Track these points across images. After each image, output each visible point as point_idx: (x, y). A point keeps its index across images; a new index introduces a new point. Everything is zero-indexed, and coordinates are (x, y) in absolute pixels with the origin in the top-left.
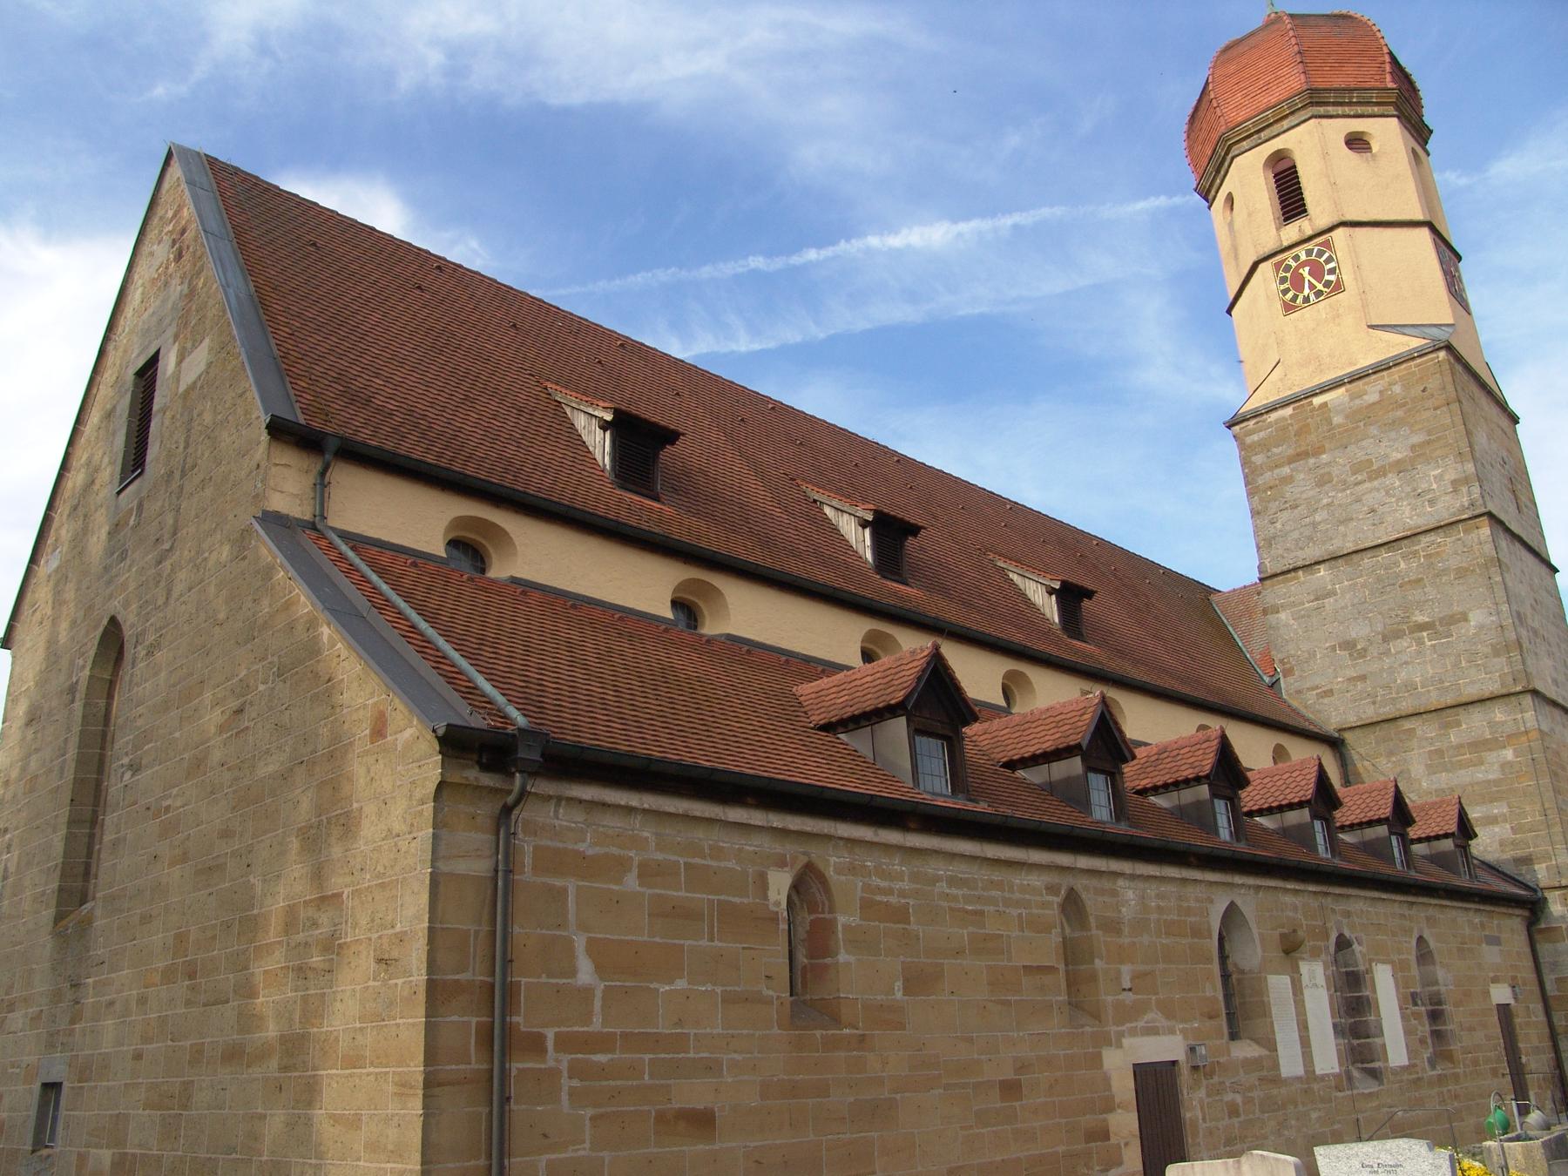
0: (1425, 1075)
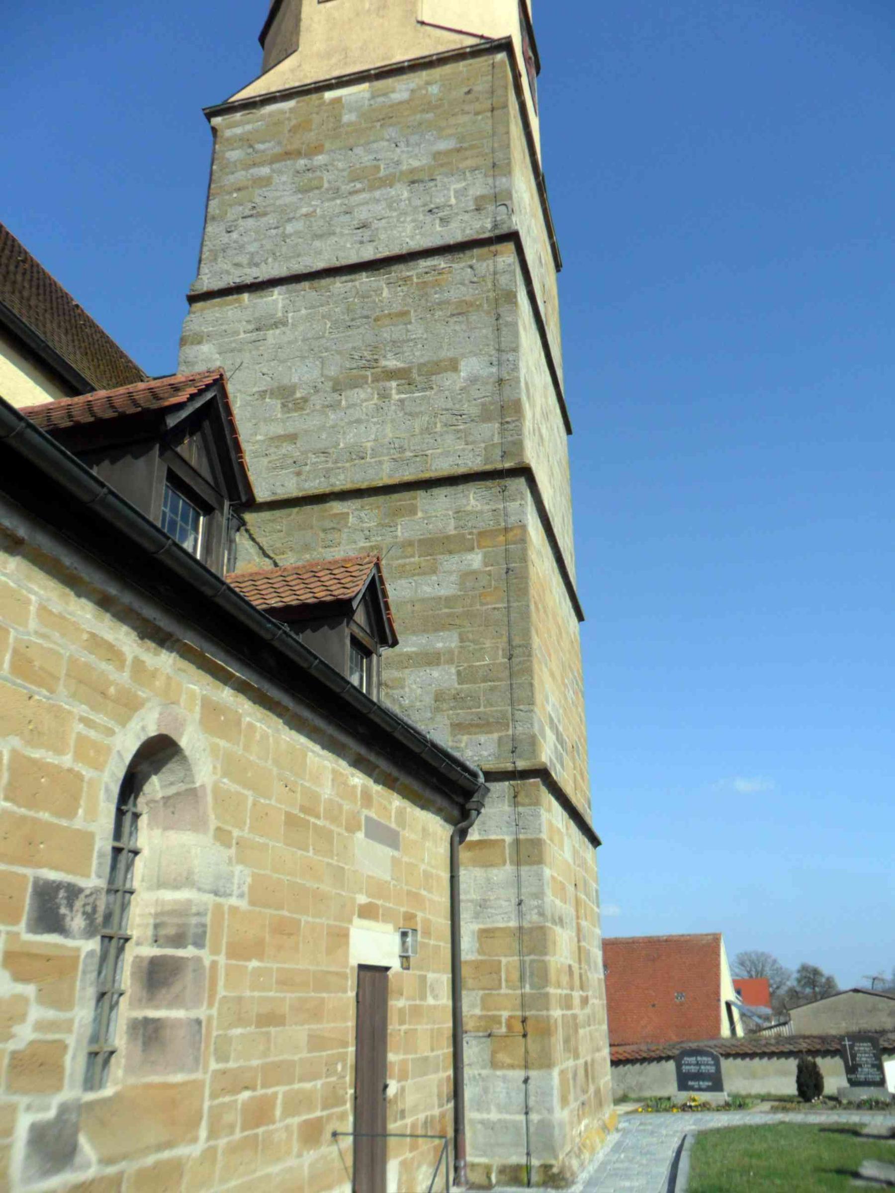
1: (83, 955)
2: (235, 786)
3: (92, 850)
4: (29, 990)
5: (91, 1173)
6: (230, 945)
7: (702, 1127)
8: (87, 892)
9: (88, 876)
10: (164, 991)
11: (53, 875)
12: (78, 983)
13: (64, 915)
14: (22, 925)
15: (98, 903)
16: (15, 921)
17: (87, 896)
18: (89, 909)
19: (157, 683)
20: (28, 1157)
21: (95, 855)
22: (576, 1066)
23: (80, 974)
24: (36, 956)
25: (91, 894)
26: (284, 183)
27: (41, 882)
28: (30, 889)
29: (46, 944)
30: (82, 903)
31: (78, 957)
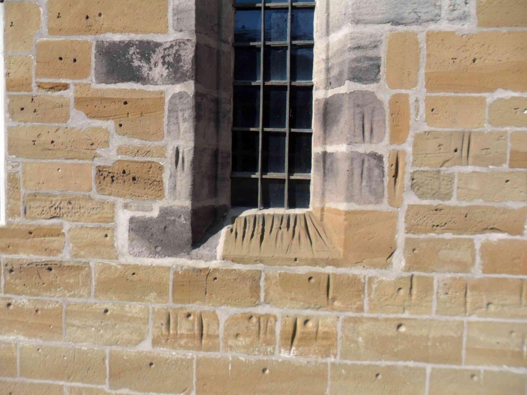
0: (94, 263)
1: (167, 100)
2: (44, 257)
3: (166, 9)
4: (110, 125)
5: (213, 264)
6: (428, 78)
7: (474, 170)
8: (168, 45)
9: (165, 31)
10: (335, 128)
11: (117, 38)
12: (165, 120)
13: (139, 67)
14: (92, 77)
15: (182, 53)
16: (85, 75)
17: (165, 49)
18: (170, 59)
19: (120, 349)
20: (131, 240)
21: (170, 10)
22: (324, 143)
23: (166, 112)
24: (113, 100)
25: (172, 46)
26: (130, 307)
27: (106, 45)
28: (94, 51)
29: (121, 90)
30: (161, 55)
31: (162, 99)
